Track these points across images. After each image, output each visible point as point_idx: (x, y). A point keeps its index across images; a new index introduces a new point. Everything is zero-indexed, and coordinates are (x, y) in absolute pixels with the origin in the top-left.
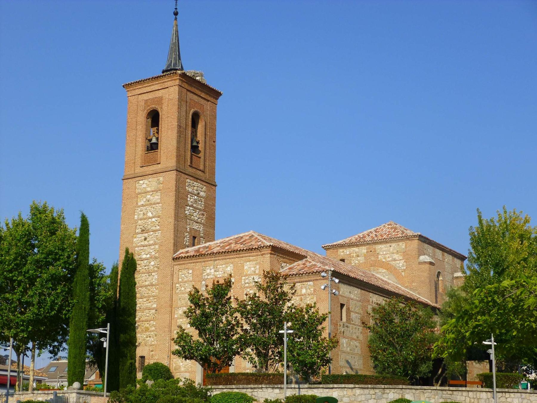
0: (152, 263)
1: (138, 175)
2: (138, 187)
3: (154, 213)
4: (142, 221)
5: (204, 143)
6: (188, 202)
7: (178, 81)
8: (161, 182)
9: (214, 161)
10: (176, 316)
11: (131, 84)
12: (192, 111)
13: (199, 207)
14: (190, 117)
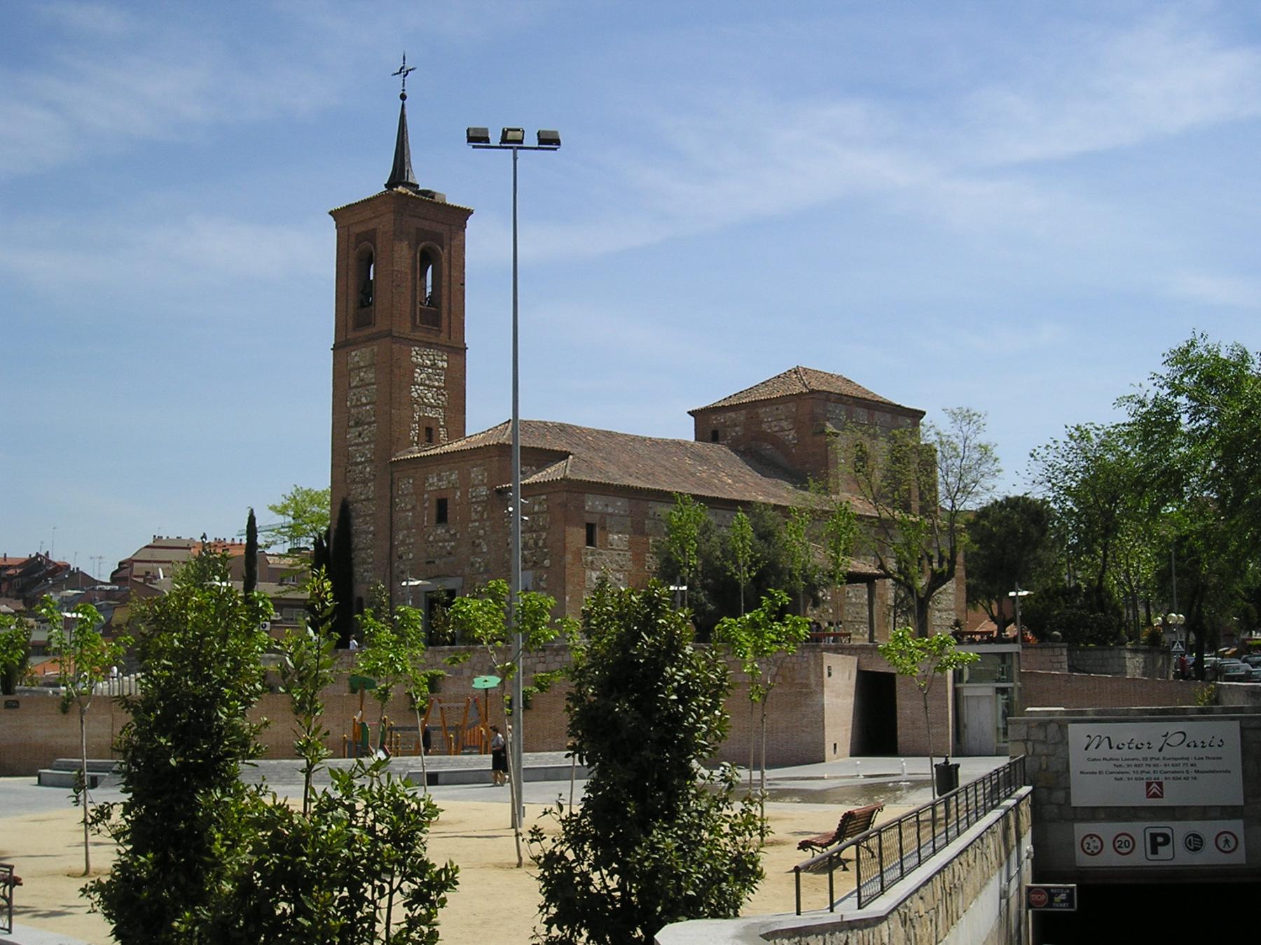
0: (368, 469)
10: (396, 543)
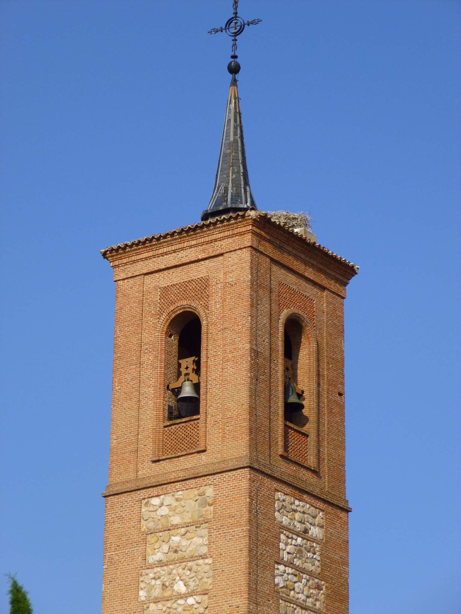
1: (147, 483)
2: (146, 515)
3: (192, 584)
4: (160, 606)
5: (314, 397)
6: (281, 552)
7: (249, 236)
8: (210, 501)
9: (341, 445)
11: (124, 249)
12: (285, 314)
13: (309, 566)
14: (281, 329)
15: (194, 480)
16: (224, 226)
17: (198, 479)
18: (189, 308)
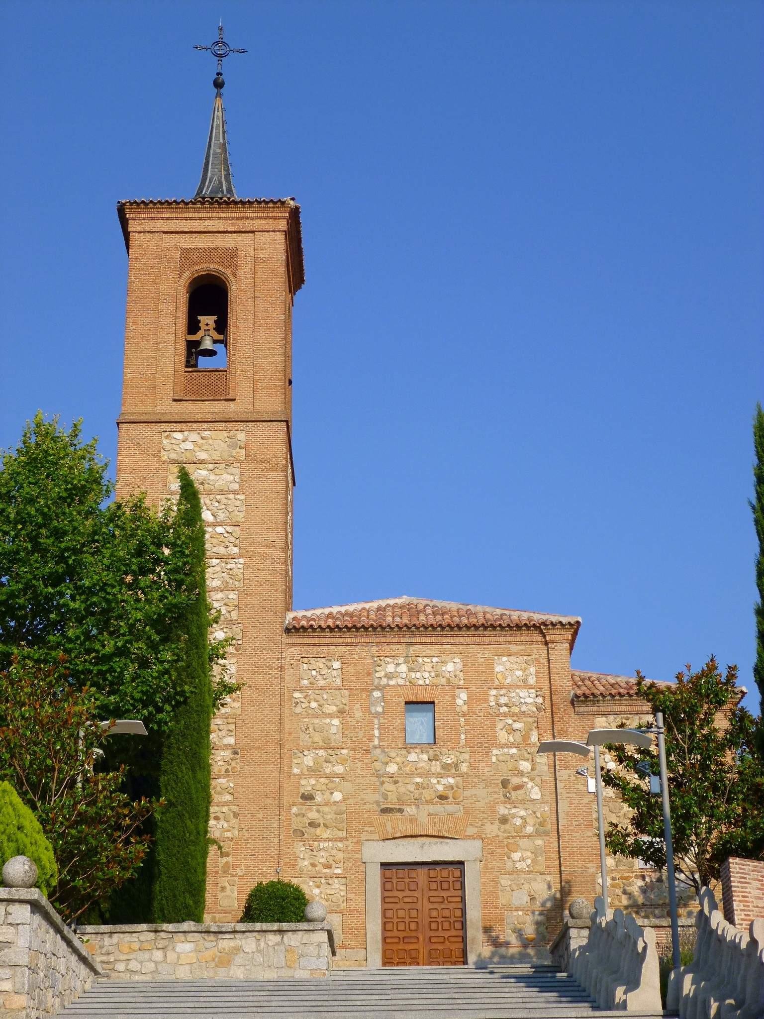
15: (224, 424)
16: (261, 207)
17: (228, 423)
18: (214, 271)
